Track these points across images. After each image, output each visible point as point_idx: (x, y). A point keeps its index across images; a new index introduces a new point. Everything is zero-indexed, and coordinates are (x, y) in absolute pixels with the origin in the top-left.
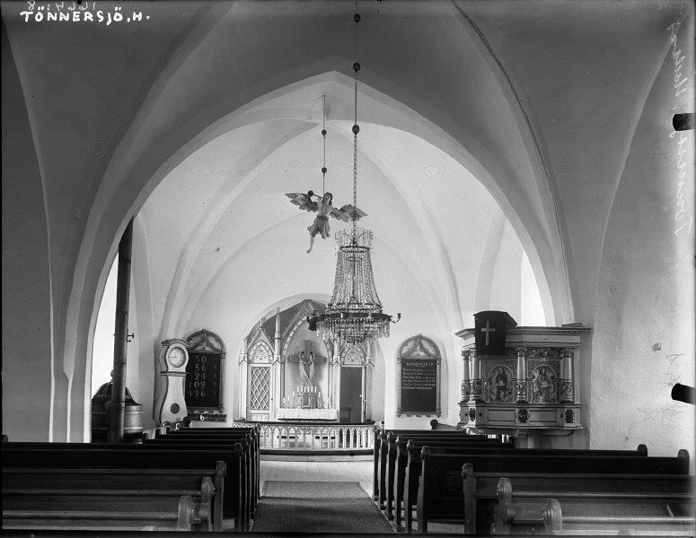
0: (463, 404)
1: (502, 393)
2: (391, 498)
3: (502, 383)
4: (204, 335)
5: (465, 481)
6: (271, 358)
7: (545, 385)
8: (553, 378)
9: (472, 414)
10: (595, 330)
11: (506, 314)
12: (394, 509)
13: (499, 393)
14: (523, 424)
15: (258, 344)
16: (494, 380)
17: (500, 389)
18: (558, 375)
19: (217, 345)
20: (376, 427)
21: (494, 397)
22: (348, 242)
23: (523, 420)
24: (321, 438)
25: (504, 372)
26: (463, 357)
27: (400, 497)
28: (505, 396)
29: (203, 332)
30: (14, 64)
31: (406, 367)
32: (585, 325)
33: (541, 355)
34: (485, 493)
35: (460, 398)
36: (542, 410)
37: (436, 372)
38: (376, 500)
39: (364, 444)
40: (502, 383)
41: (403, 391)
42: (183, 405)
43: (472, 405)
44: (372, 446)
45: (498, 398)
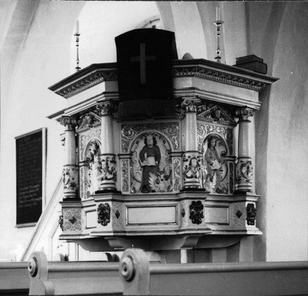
1: (152, 179)
3: (151, 161)
8: (223, 155)
13: (146, 178)
14: (196, 226)
16: (136, 158)
17: (146, 170)
18: (232, 150)
20: (216, 109)
21: (138, 186)
22: (65, 172)
23: (197, 217)
25: (155, 142)
28: (157, 182)
30: (239, 254)
33: (137, 143)
36: (220, 204)
40: (151, 161)
42: (173, 160)
45: (145, 188)
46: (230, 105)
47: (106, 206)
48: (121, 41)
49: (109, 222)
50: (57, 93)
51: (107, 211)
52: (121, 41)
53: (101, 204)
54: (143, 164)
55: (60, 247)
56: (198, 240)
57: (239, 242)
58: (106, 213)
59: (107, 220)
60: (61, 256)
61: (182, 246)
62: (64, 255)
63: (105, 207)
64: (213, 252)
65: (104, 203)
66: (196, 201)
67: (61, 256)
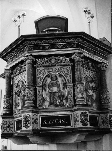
46: (66, 54)
47: (28, 116)
48: (37, 23)
49: (30, 126)
50: (111, 50)
51: (29, 119)
52: (37, 23)
53: (25, 115)
54: (50, 91)
55: (3, 141)
56: (85, 136)
57: (102, 138)
58: (28, 120)
59: (29, 125)
60: (3, 146)
61: (75, 140)
62: (5, 146)
63: (27, 116)
64: (88, 143)
65: (26, 114)
66: (84, 111)
67: (3, 146)
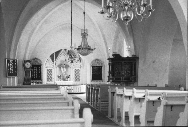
0: (109, 77)
2: (92, 101)
4: (35, 59)
5: (109, 89)
6: (53, 66)
7: (128, 71)
9: (111, 79)
10: (140, 57)
11: (119, 54)
12: (92, 102)
15: (49, 62)
19: (39, 62)
24: (71, 89)
26: (108, 65)
27: (92, 101)
29: (36, 58)
31: (93, 68)
32: (137, 56)
34: (112, 91)
35: (108, 75)
37: (102, 69)
38: (87, 102)
39: (80, 91)
41: (93, 75)
43: (111, 77)
44: (85, 91)
